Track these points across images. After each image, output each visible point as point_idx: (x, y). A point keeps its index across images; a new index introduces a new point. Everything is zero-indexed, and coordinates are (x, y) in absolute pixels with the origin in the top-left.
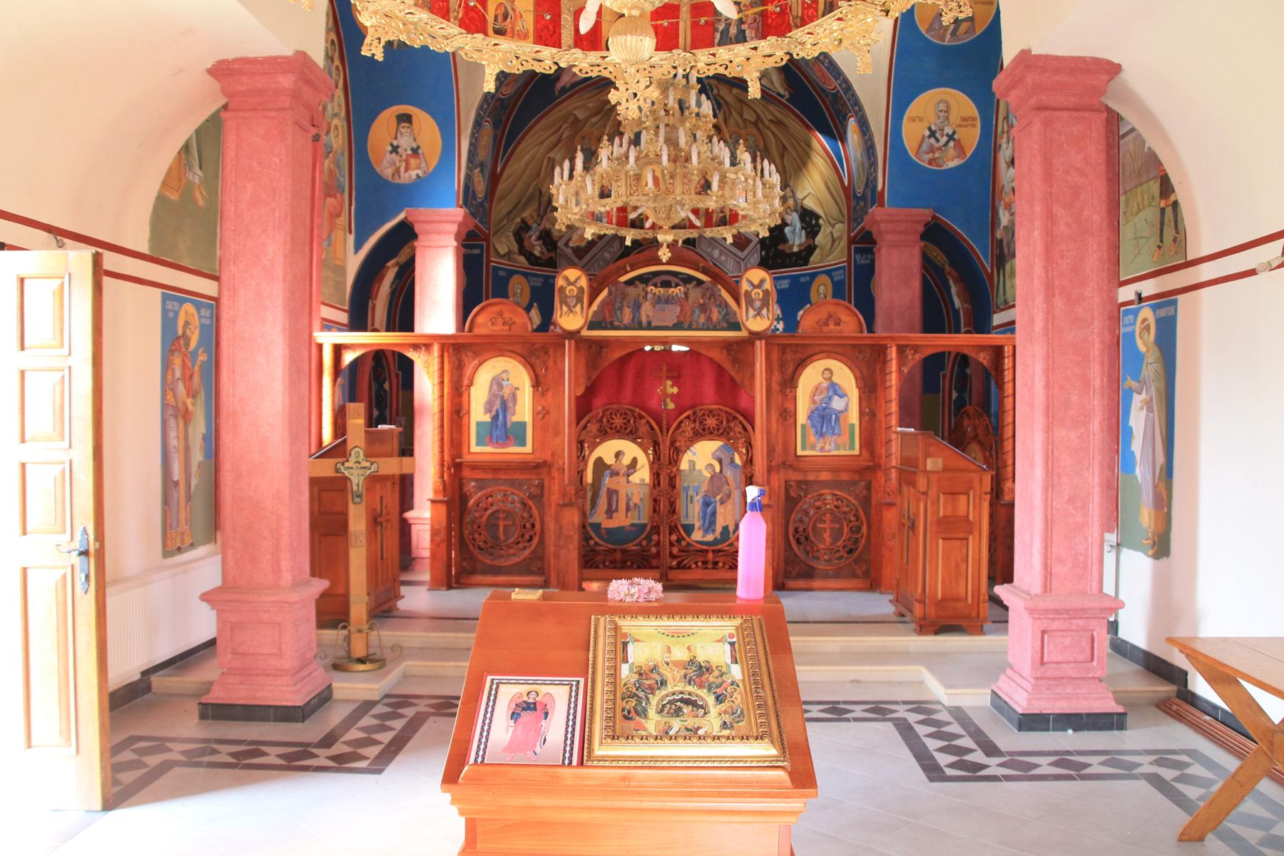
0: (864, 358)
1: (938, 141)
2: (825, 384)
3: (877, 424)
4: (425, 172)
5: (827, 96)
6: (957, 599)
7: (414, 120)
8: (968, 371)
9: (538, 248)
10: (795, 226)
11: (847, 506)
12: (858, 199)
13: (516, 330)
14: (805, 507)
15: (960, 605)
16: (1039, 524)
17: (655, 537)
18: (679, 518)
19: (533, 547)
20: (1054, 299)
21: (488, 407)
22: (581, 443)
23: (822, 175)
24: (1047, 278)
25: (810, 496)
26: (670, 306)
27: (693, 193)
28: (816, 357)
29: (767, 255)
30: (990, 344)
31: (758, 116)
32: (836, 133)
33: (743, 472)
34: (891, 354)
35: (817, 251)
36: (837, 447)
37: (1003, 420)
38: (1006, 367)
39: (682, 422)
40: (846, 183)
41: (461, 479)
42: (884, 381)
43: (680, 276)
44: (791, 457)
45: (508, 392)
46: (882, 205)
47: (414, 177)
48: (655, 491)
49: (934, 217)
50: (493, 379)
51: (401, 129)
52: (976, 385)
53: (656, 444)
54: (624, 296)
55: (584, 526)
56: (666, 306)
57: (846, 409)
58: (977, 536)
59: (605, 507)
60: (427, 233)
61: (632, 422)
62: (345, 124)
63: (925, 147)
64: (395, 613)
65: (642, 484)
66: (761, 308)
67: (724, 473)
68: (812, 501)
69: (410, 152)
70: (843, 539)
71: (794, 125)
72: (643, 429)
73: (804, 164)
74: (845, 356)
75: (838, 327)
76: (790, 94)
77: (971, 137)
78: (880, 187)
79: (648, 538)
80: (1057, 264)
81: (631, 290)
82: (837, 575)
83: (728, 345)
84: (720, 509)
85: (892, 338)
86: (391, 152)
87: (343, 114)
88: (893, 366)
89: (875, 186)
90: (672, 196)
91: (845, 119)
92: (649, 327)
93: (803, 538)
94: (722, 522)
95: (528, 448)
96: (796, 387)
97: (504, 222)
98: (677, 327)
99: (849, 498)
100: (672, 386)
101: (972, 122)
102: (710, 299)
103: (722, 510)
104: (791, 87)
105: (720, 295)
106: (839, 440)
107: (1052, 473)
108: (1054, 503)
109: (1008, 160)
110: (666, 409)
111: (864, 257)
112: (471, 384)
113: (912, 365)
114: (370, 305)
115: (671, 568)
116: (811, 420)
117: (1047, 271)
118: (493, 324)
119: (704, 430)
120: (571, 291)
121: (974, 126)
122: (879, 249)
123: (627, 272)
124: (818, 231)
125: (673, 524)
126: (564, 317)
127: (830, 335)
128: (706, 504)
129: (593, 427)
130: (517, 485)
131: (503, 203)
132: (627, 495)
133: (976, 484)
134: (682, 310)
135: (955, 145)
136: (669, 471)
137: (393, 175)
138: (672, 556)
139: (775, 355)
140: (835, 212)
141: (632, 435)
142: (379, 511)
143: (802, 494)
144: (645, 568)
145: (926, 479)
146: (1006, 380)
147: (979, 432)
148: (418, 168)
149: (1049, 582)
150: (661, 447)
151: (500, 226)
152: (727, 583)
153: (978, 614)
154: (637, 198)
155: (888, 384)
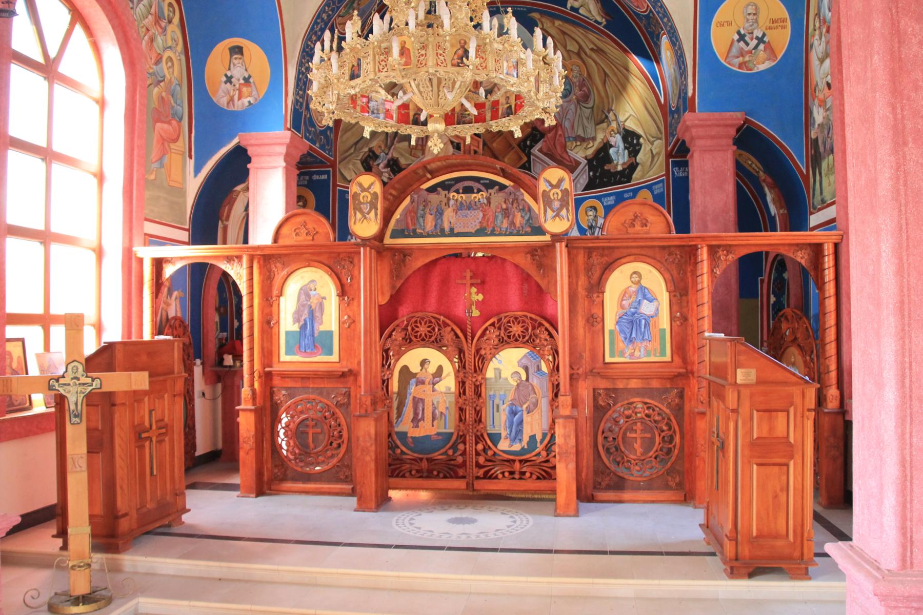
0: (675, 259)
1: (747, 44)
2: (634, 288)
3: (689, 329)
4: (256, 99)
5: (641, 19)
6: (777, 536)
7: (244, 50)
8: (785, 275)
9: (387, 175)
10: (619, 147)
11: (659, 414)
12: (672, 113)
13: (320, 240)
14: (615, 415)
15: (779, 543)
16: (892, 469)
17: (461, 447)
18: (485, 427)
19: (341, 455)
20: (906, 149)
21: (297, 318)
22: (387, 351)
23: (640, 97)
24: (895, 120)
25: (619, 405)
26: (473, 212)
27: (449, 65)
28: (624, 260)
29: (594, 174)
30: (808, 241)
31: (580, 47)
32: (650, 54)
33: (550, 381)
34: (702, 254)
35: (639, 168)
36: (648, 354)
37: (824, 323)
38: (826, 266)
39: (486, 329)
40: (662, 101)
41: (271, 388)
42: (695, 283)
43: (482, 182)
44: (599, 364)
45: (315, 302)
46: (693, 110)
47: (247, 104)
48: (460, 400)
49: (746, 121)
50: (301, 289)
51: (234, 61)
52: (794, 288)
53: (461, 352)
54: (426, 203)
55: (390, 435)
56: (469, 212)
57: (657, 314)
58: (800, 461)
59: (412, 416)
60: (260, 155)
61: (436, 330)
62: (183, 58)
63: (734, 51)
64: (176, 529)
65: (448, 393)
66: (560, 209)
67: (530, 381)
68: (622, 410)
69: (242, 81)
70: (655, 449)
71: (612, 50)
72: (448, 337)
73: (624, 88)
74: (654, 259)
75: (645, 228)
76: (607, 20)
77: (782, 38)
78: (690, 93)
79: (454, 447)
80: (908, 99)
81: (433, 197)
82: (649, 485)
83: (532, 250)
84: (527, 418)
85: (703, 238)
86: (226, 83)
87: (180, 47)
88: (705, 267)
89: (686, 93)
90: (425, 69)
91: (658, 38)
92: (452, 234)
93: (615, 450)
94: (529, 431)
95: (335, 358)
96: (603, 292)
97: (352, 150)
98: (480, 232)
99: (660, 406)
100: (477, 293)
101: (781, 24)
102: (512, 204)
103: (529, 419)
104: (607, 14)
105: (523, 200)
106: (650, 346)
107: (911, 396)
108: (914, 440)
109: (820, 55)
110: (471, 317)
111: (681, 170)
112: (281, 294)
113: (725, 266)
114: (220, 225)
115: (478, 478)
116: (620, 326)
117: (894, 109)
118: (297, 234)
119: (509, 337)
120: (365, 197)
121: (784, 27)
122: (692, 156)
123: (429, 180)
124: (640, 150)
125: (479, 434)
126: (358, 225)
127: (636, 236)
128: (513, 413)
129: (398, 336)
130: (325, 394)
131: (349, 134)
132: (433, 404)
133: (798, 400)
134: (484, 216)
135: (765, 48)
136: (474, 380)
137: (228, 103)
138: (479, 466)
139: (581, 259)
140: (653, 130)
141: (437, 344)
142: (147, 424)
143: (611, 402)
144: (452, 477)
145: (736, 394)
146: (827, 280)
147: (798, 335)
148: (250, 96)
149: (908, 554)
150: (466, 354)
151: (347, 154)
152: (535, 493)
153: (802, 554)
154: (386, 74)
155: (699, 287)
